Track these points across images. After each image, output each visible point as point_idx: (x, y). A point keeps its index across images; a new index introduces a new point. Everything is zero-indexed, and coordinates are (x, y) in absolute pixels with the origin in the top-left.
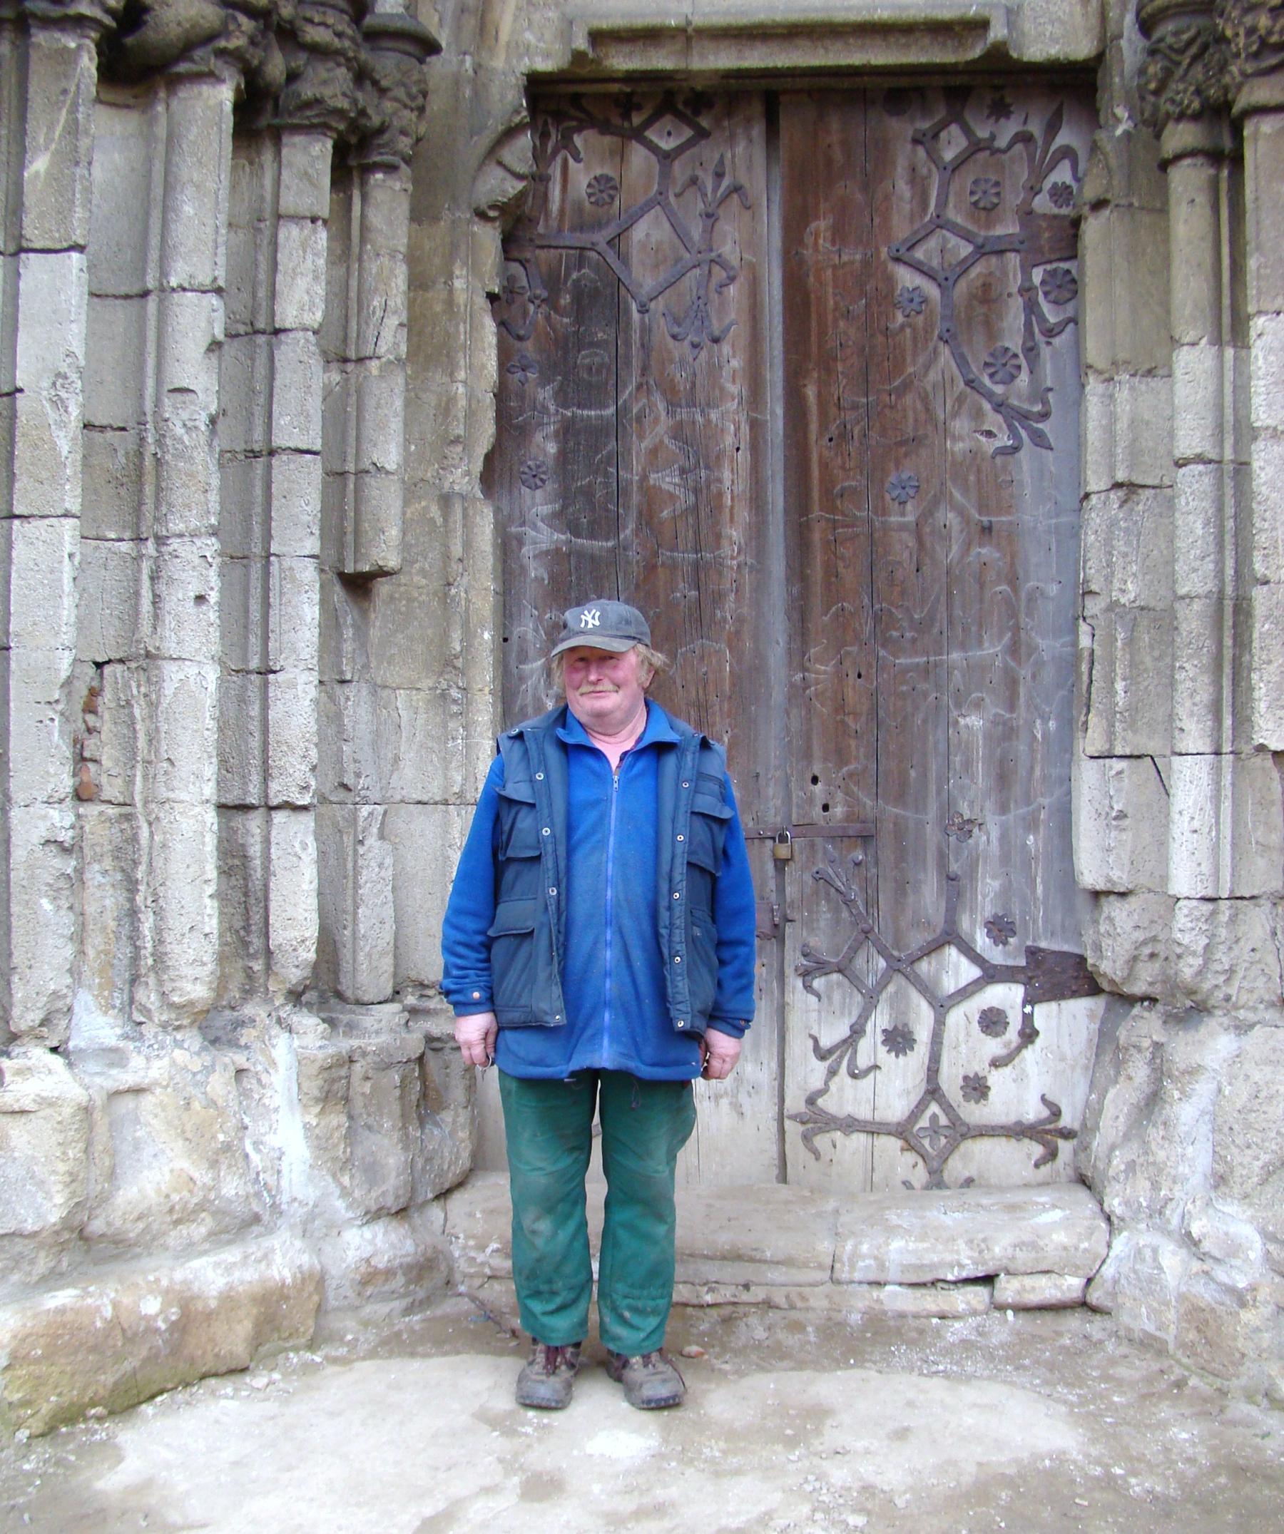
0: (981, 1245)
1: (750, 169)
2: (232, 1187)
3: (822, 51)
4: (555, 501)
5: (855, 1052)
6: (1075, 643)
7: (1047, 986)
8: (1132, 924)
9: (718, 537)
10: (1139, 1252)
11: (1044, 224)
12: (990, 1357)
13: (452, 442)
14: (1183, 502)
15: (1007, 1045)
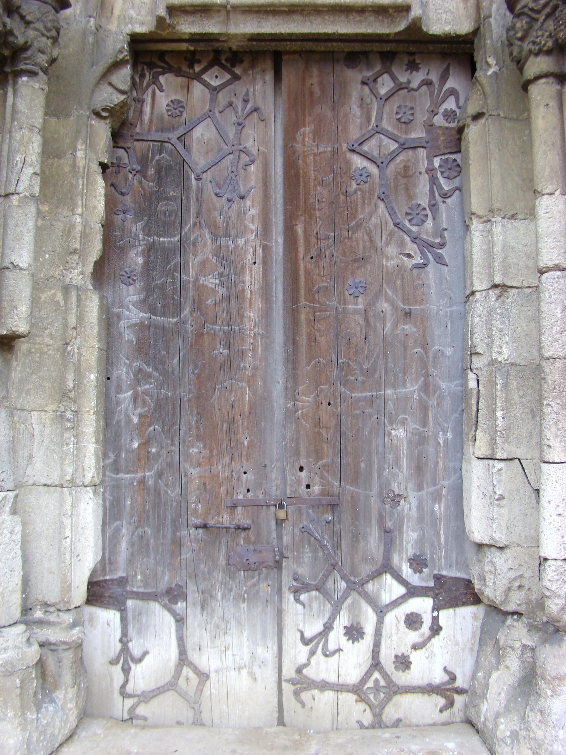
1: (264, 98)
3: (308, 24)
4: (141, 293)
5: (327, 641)
6: (465, 384)
7: (447, 599)
8: (507, 567)
9: (242, 316)
11: (440, 132)
13: (71, 253)
14: (547, 295)
15: (422, 635)
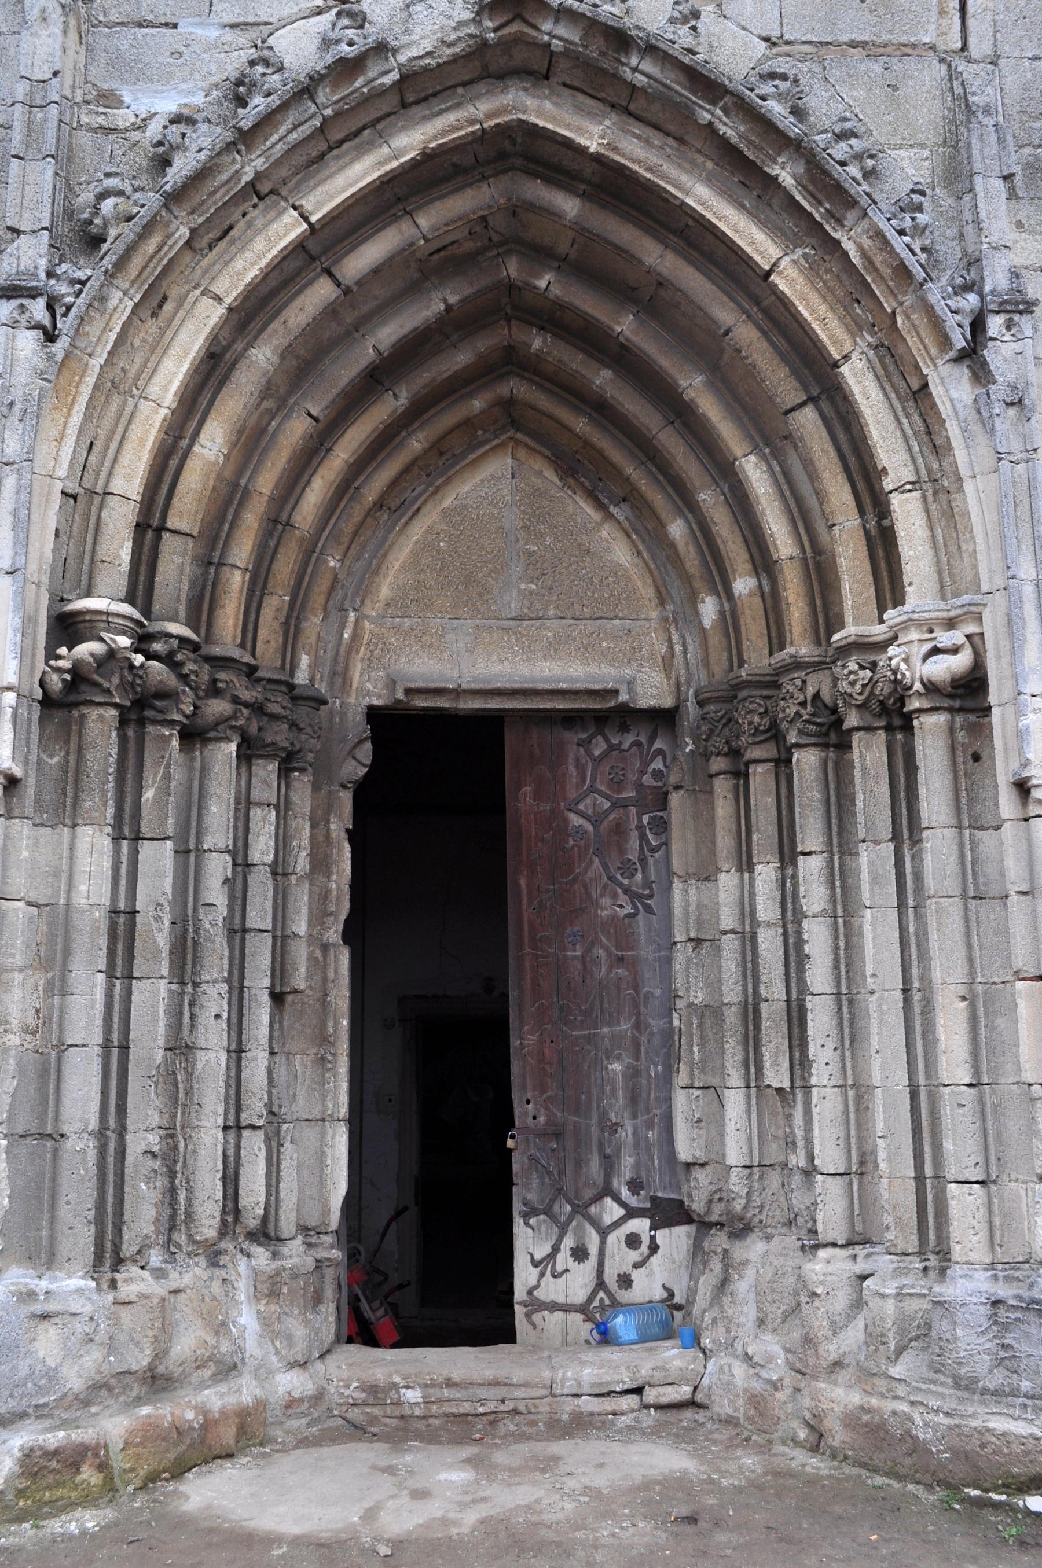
0: (634, 1370)
2: (225, 1347)
6: (671, 1022)
10: (721, 1368)
12: (643, 1433)
15: (642, 1254)
